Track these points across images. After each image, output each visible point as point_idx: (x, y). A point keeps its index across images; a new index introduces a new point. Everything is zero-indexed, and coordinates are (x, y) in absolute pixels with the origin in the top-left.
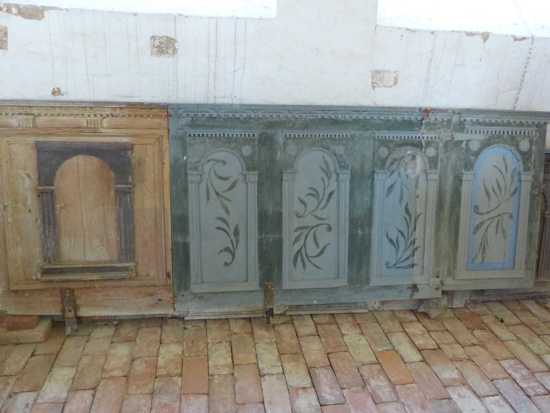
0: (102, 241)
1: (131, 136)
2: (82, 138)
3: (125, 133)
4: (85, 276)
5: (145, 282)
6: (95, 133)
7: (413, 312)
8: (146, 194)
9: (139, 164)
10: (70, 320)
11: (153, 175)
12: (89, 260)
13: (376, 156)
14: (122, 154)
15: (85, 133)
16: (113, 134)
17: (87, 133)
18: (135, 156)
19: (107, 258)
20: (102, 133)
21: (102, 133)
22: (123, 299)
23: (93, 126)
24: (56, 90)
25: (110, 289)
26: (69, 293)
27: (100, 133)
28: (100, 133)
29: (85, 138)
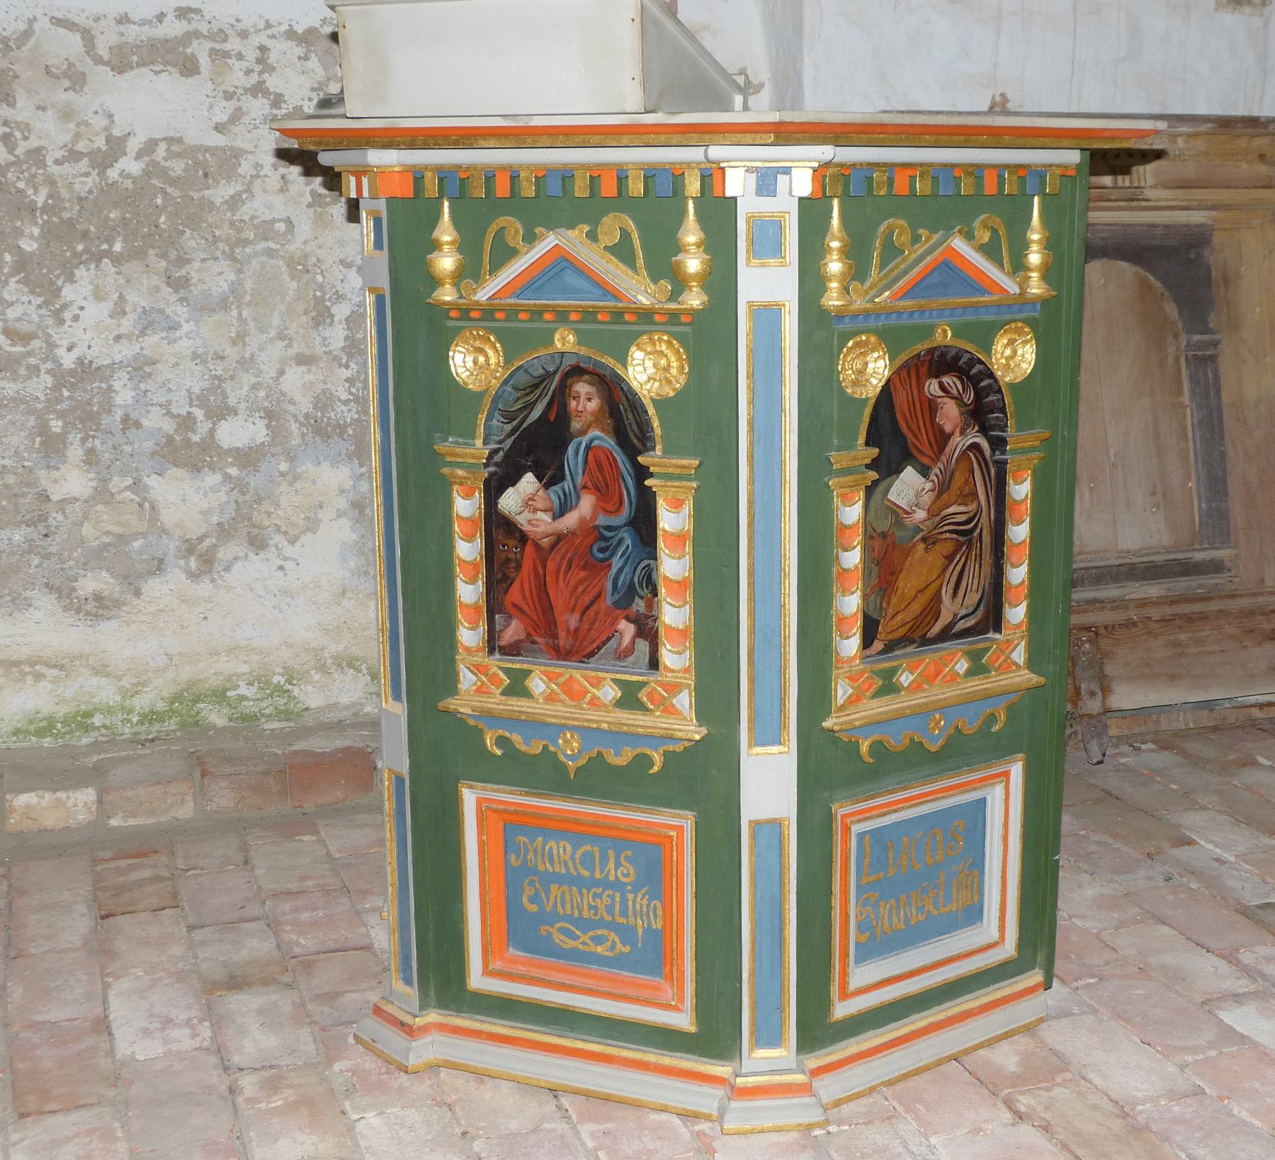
0: (1154, 493)
1: (1213, 208)
2: (1104, 214)
3: (1197, 200)
4: (1125, 591)
5: (1261, 599)
6: (1133, 200)
7: (1259, 922)
8: (1244, 362)
9: (1226, 282)
10: (1093, 722)
11: (1258, 310)
12: (1125, 548)
13: (259, 696)
14: (1192, 256)
15: (1110, 200)
16: (1160, 204)
17: (1115, 200)
18: (1219, 255)
19: (1167, 539)
20: (1147, 200)
21: (1147, 200)
22: (1210, 653)
23: (1136, 184)
24: (998, 99)
25: (1180, 627)
26: (1088, 641)
27: (1144, 200)
28: (1144, 200)
29: (1110, 214)
